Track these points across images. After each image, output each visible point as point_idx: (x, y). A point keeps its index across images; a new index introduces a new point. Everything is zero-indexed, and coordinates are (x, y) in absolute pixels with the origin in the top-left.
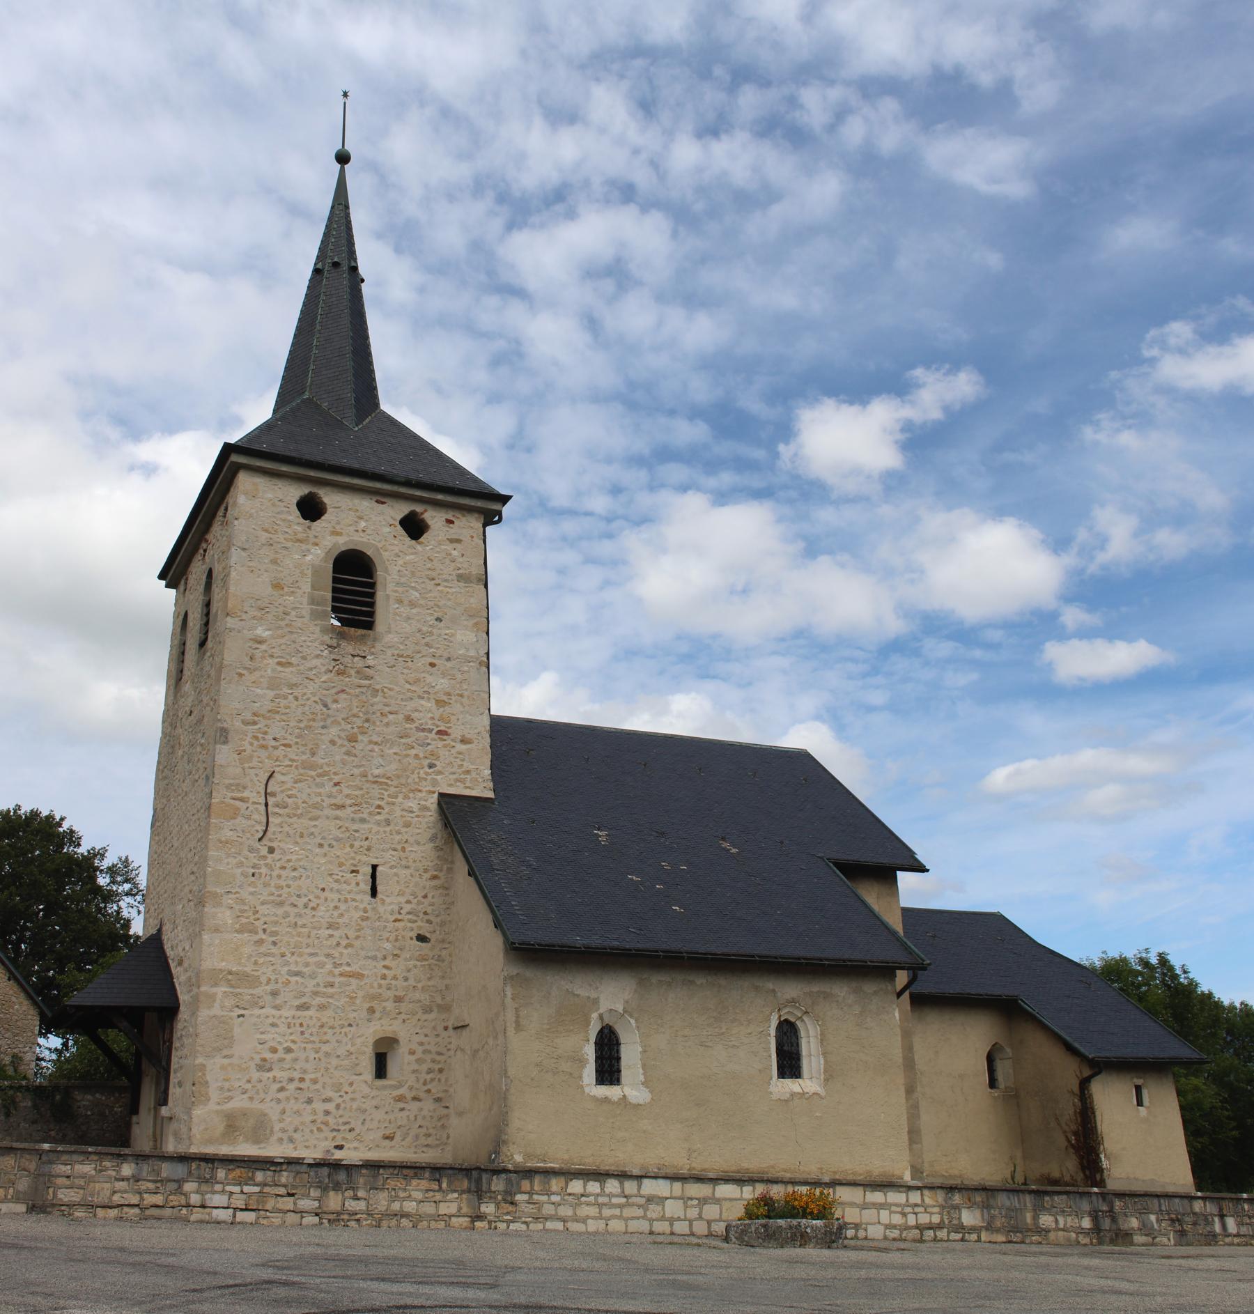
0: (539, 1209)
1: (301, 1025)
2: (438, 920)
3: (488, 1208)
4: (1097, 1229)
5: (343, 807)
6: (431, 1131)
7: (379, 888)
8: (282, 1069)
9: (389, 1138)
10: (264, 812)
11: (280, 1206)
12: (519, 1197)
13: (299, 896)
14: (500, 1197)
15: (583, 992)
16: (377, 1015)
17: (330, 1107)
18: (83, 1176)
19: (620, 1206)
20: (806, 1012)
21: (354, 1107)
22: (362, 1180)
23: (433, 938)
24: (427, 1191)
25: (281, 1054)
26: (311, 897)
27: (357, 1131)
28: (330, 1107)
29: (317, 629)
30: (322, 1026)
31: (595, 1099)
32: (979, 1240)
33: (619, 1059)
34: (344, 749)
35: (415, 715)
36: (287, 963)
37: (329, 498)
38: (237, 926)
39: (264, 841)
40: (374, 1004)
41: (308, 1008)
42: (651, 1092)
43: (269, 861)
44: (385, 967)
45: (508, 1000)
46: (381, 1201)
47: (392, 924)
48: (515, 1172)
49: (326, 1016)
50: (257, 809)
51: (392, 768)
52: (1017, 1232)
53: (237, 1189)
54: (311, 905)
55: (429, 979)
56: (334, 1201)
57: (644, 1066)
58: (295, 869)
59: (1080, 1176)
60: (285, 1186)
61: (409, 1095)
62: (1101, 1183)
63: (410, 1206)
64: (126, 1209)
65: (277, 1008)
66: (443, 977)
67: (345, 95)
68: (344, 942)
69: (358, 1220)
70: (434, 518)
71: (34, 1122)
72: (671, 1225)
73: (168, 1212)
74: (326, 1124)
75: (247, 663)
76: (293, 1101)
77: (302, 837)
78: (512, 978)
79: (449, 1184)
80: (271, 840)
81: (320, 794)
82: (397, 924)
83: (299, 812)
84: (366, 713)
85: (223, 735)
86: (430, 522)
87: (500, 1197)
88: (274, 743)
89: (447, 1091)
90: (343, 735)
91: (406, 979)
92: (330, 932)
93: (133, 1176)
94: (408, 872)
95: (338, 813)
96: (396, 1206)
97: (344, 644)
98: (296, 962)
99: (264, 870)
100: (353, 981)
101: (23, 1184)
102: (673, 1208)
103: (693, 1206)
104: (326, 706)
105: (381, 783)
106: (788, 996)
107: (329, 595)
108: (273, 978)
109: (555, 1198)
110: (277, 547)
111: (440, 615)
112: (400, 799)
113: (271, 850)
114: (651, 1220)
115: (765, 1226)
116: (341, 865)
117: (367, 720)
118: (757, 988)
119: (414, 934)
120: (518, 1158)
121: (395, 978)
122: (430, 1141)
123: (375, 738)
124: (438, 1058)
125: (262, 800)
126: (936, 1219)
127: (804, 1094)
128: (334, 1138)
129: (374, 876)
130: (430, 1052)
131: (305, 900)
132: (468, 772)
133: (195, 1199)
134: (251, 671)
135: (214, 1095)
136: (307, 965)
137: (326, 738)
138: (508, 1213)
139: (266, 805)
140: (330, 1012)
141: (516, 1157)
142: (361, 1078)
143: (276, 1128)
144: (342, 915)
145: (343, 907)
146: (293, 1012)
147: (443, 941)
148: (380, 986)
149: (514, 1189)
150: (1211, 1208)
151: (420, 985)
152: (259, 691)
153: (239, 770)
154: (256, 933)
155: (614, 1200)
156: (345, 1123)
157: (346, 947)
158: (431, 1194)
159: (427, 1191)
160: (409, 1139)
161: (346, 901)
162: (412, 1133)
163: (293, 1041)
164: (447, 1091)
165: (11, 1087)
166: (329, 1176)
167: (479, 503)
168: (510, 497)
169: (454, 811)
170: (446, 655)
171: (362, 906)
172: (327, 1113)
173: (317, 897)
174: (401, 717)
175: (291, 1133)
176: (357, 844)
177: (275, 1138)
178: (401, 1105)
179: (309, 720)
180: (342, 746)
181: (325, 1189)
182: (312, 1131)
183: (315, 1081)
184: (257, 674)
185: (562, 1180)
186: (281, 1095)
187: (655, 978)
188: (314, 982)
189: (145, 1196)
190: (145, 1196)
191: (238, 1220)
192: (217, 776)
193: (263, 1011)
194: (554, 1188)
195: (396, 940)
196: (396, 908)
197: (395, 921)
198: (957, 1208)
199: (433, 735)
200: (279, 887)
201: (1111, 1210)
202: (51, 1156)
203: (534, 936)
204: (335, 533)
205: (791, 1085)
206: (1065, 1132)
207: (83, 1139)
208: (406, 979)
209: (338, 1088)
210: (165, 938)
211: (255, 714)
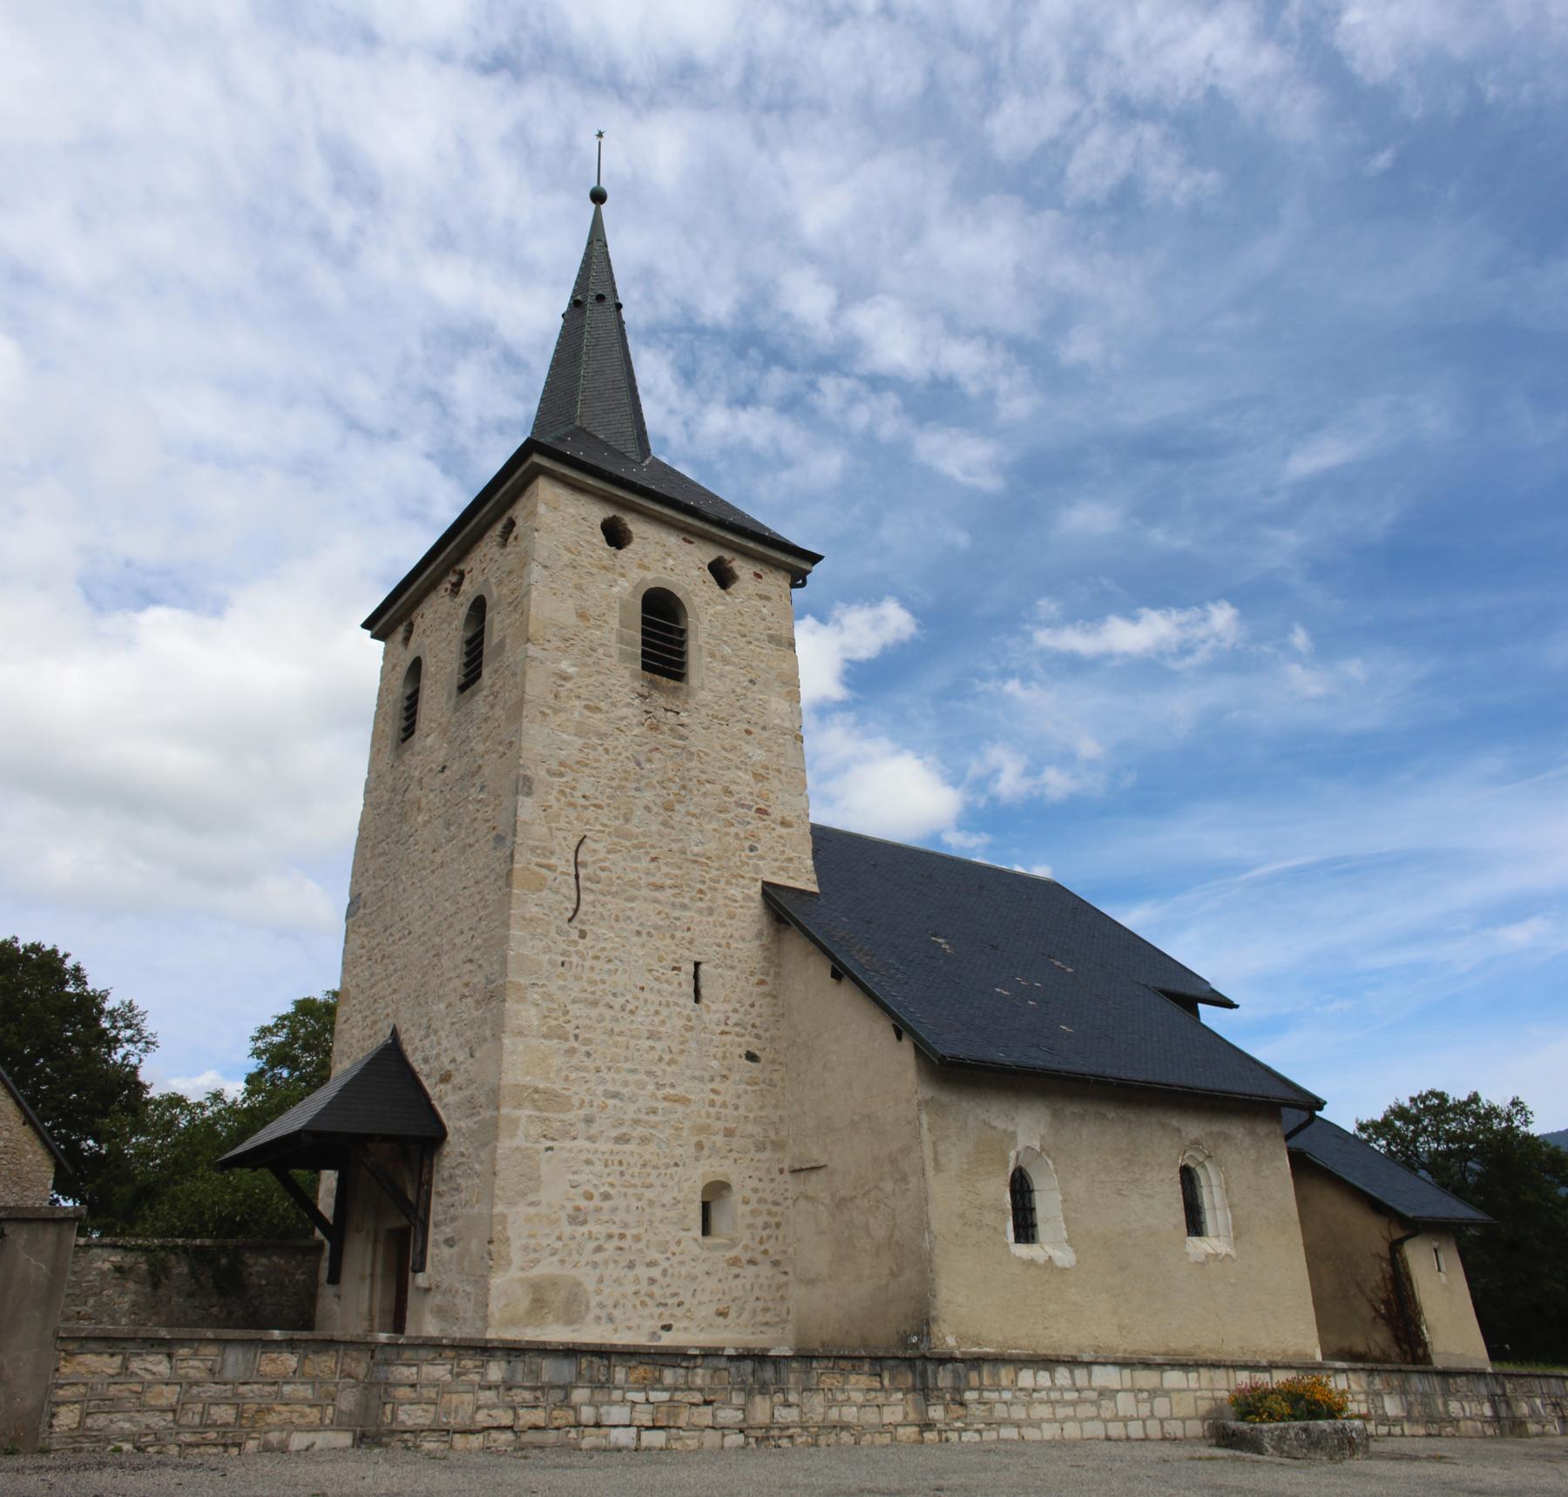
0: (991, 1411)
1: (620, 1163)
2: (767, 1035)
3: (936, 1413)
4: (1496, 1418)
5: (661, 887)
6: (770, 1305)
7: (703, 991)
8: (599, 1222)
9: (722, 1314)
10: (573, 886)
11: (696, 1420)
13: (615, 995)
14: (948, 1397)
15: (999, 1124)
16: (706, 1152)
17: (656, 1272)
18: (435, 1384)
19: (1074, 1404)
20: (1209, 1157)
21: (683, 1273)
22: (792, 1378)
24: (868, 1390)
25: (597, 1201)
26: (629, 997)
27: (687, 1306)
28: (656, 1272)
29: (627, 674)
30: (644, 1165)
31: (1020, 1260)
33: (1032, 1210)
34: (660, 819)
35: (733, 787)
36: (603, 1081)
37: (635, 525)
38: (544, 1029)
39: (575, 923)
41: (627, 1141)
42: (1076, 1252)
43: (580, 948)
44: (713, 1091)
45: (924, 1131)
46: (816, 1406)
47: (717, 1038)
48: (962, 1361)
49: (649, 1151)
50: (566, 882)
51: (712, 847)
52: (1509, 1426)
53: (640, 1397)
54: (630, 1007)
55: (762, 1108)
56: (761, 1409)
57: (1066, 1220)
58: (610, 961)
59: (1394, 1351)
60: (701, 1390)
62: (1426, 1359)
63: (850, 1414)
64: (494, 1434)
65: (592, 1139)
66: (776, 1107)
67: (600, 135)
68: (667, 1057)
69: (791, 1437)
70: (743, 569)
71: (191, 1295)
72: (1126, 1426)
73: (551, 1436)
74: (651, 1296)
75: (552, 701)
76: (612, 1265)
77: (617, 920)
78: (926, 1102)
80: (582, 922)
81: (635, 870)
82: (724, 1037)
83: (614, 889)
84: (682, 779)
85: (525, 785)
86: (738, 573)
87: (948, 1397)
88: (583, 801)
89: (785, 1252)
90: (658, 801)
91: (736, 1108)
92: (651, 1043)
93: (504, 1382)
94: (734, 973)
95: (657, 894)
96: (834, 1414)
97: (656, 695)
98: (614, 1081)
99: (575, 959)
100: (679, 1107)
101: (348, 1400)
102: (1125, 1404)
103: (1144, 1401)
104: (639, 764)
105: (702, 864)
106: (1192, 1137)
107: (639, 636)
108: (587, 1099)
109: (1007, 1395)
110: (573, 576)
111: (753, 676)
112: (722, 885)
113: (583, 935)
114: (1105, 1421)
115: (1305, 1430)
116: (661, 959)
117: (684, 787)
118: (1163, 1125)
119: (742, 1051)
120: (951, 1341)
121: (724, 1105)
122: (768, 1317)
123: (692, 809)
124: (775, 1209)
125: (572, 870)
126: (1364, 1410)
127: (1217, 1255)
128: (661, 1315)
129: (696, 977)
130: (765, 1201)
131: (621, 1000)
132: (790, 860)
133: (587, 1414)
134: (557, 711)
135: (517, 1257)
136: (626, 1084)
137: (641, 803)
138: (958, 1418)
139: (577, 877)
140: (652, 1148)
141: (948, 1339)
142: (690, 1234)
143: (593, 1303)
145: (665, 1012)
146: (611, 1146)
147: (773, 1062)
148: (708, 1115)
149: (963, 1386)
151: (751, 1116)
152: (565, 736)
153: (545, 830)
154: (567, 1039)
156: (675, 1295)
157: (669, 1064)
158: (873, 1394)
159: (868, 1390)
160: (746, 1316)
161: (668, 1005)
162: (748, 1308)
163: (612, 1185)
164: (785, 1252)
165: (162, 1247)
166: (754, 1373)
167: (790, 560)
168: (820, 558)
169: (780, 907)
170: (761, 723)
171: (685, 1013)
172: (652, 1281)
173: (637, 998)
174: (718, 788)
175: (610, 1309)
176: (678, 934)
177: (590, 1316)
178: (735, 1270)
179: (622, 779)
180: (657, 814)
181: (750, 1393)
182: (634, 1307)
183: (637, 1239)
184: (563, 716)
185: (1011, 1368)
186: (598, 1257)
187: (1071, 1109)
188: (633, 1107)
189: (521, 1412)
190: (521, 1412)
191: (644, 1444)
192: (520, 834)
193: (576, 1143)
194: (1005, 1382)
195: (724, 1057)
196: (723, 1018)
197: (722, 1033)
198: (1378, 1394)
199: (752, 813)
200: (592, 982)
201: (1504, 1394)
202: (391, 1354)
203: (950, 1045)
204: (642, 567)
205: (1022, 1250)
206: (1370, 1301)
207: (256, 1320)
208: (736, 1108)
209: (663, 1247)
210: (408, 1049)
211: (561, 764)
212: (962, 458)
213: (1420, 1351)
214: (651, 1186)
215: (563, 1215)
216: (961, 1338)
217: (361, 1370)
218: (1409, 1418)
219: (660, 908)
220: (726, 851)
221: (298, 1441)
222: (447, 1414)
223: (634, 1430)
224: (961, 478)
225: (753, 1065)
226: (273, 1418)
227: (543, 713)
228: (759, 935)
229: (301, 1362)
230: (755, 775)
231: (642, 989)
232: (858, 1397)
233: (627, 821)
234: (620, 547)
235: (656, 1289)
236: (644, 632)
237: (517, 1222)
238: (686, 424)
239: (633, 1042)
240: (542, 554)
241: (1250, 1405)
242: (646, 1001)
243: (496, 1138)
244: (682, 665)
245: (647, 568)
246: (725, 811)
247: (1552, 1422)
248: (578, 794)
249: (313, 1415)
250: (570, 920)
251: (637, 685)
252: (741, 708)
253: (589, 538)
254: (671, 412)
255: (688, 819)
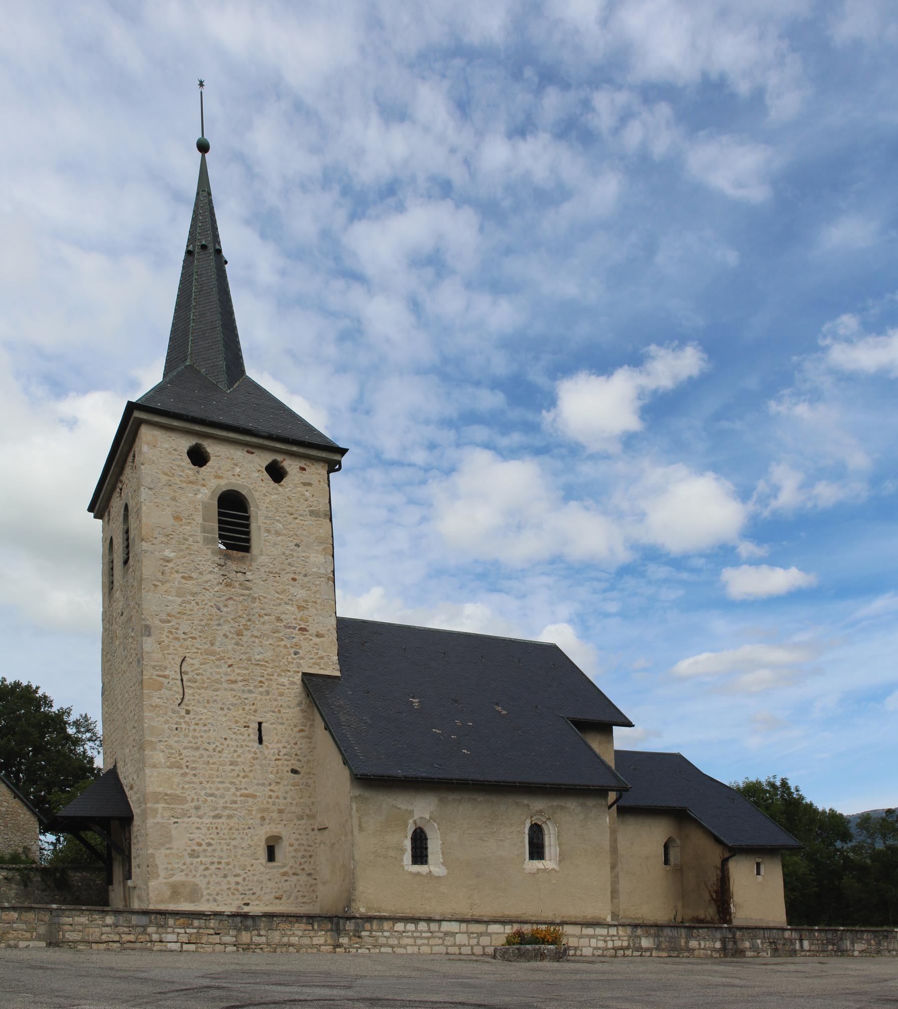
0: (376, 940)
1: (217, 828)
2: (305, 759)
3: (344, 940)
4: (724, 948)
5: (235, 682)
6: (306, 894)
7: (264, 738)
8: (206, 856)
9: (279, 898)
10: (180, 685)
11: (211, 940)
12: (363, 933)
13: (209, 743)
15: (403, 806)
16: (267, 821)
17: (239, 879)
22: (262, 925)
23: (302, 771)
25: (204, 847)
26: (217, 744)
27: (258, 894)
28: (239, 879)
31: (411, 873)
32: (651, 956)
33: (426, 848)
34: (234, 641)
36: (205, 788)
38: (168, 764)
39: (183, 706)
40: (265, 814)
41: (220, 818)
43: (187, 719)
44: (271, 790)
45: (354, 811)
46: (276, 937)
47: (273, 763)
49: (233, 822)
51: (269, 655)
53: (182, 931)
54: (218, 749)
55: (301, 798)
56: (245, 937)
57: (443, 853)
58: (205, 725)
61: (291, 872)
62: (729, 921)
63: (294, 940)
64: (111, 944)
65: (200, 817)
66: (310, 797)
67: (201, 84)
68: (242, 774)
70: (291, 466)
71: (44, 890)
72: (460, 949)
73: (138, 945)
74: (237, 890)
77: (208, 702)
78: (356, 797)
79: (319, 926)
80: (187, 705)
81: (219, 673)
82: (277, 762)
83: (205, 685)
84: (248, 615)
85: (147, 630)
86: (288, 470)
88: (184, 636)
92: (232, 767)
94: (283, 727)
95: (233, 686)
96: (285, 940)
97: (229, 563)
98: (211, 788)
99: (184, 726)
101: (42, 930)
102: (461, 939)
104: (219, 609)
105: (262, 665)
107: (216, 525)
108: (195, 797)
109: (386, 934)
110: (176, 488)
111: (298, 542)
112: (275, 677)
113: (188, 712)
114: (447, 946)
115: (518, 949)
117: (249, 620)
119: (289, 769)
121: (277, 797)
122: (305, 900)
123: (256, 633)
124: (308, 848)
125: (179, 677)
126: (625, 944)
129: (260, 730)
130: (303, 845)
131: (214, 746)
132: (322, 658)
134: (163, 583)
135: (162, 873)
136: (218, 789)
139: (182, 680)
140: (235, 820)
143: (205, 893)
144: (239, 756)
146: (211, 820)
148: (268, 803)
150: (795, 935)
151: (294, 802)
152: (170, 598)
153: (160, 655)
154: (182, 768)
155: (424, 935)
157: (243, 777)
160: (292, 899)
161: (242, 746)
163: (212, 839)
165: (26, 869)
166: (241, 922)
168: (347, 450)
170: (303, 572)
171: (253, 750)
172: (237, 883)
176: (247, 708)
177: (204, 899)
178: (286, 878)
179: (208, 620)
180: (233, 638)
183: (228, 864)
184: (168, 585)
186: (206, 873)
187: (451, 797)
188: (223, 801)
194: (386, 928)
195: (277, 773)
196: (276, 751)
197: (276, 760)
198: (639, 937)
199: (296, 631)
200: (195, 737)
202: (59, 912)
204: (218, 477)
206: (709, 891)
208: (285, 798)
209: (243, 868)
210: (119, 771)
211: (168, 615)
212: (733, 169)
213: (728, 918)
214: (235, 839)
215: (186, 854)
216: (368, 909)
217: (47, 918)
218: (658, 948)
219: (234, 693)
220: (278, 656)
221: (22, 944)
222: (88, 936)
223: (179, 944)
224: (731, 192)
225: (296, 776)
226: (10, 936)
227: (156, 586)
228: (300, 704)
229: (19, 916)
230: (299, 607)
231: (226, 739)
232: (300, 933)
233: (212, 644)
234: (201, 466)
235: (239, 887)
236: (220, 522)
237: (161, 857)
238: (467, 162)
239: (221, 768)
240: (147, 480)
241: (519, 939)
242: (228, 746)
243: (146, 818)
244: (248, 541)
245: (222, 478)
246: (278, 632)
247: (766, 951)
248: (180, 632)
249: (28, 935)
250: (179, 705)
251: (216, 559)
252: (289, 564)
253: (178, 463)
254: (453, 150)
255: (253, 639)
